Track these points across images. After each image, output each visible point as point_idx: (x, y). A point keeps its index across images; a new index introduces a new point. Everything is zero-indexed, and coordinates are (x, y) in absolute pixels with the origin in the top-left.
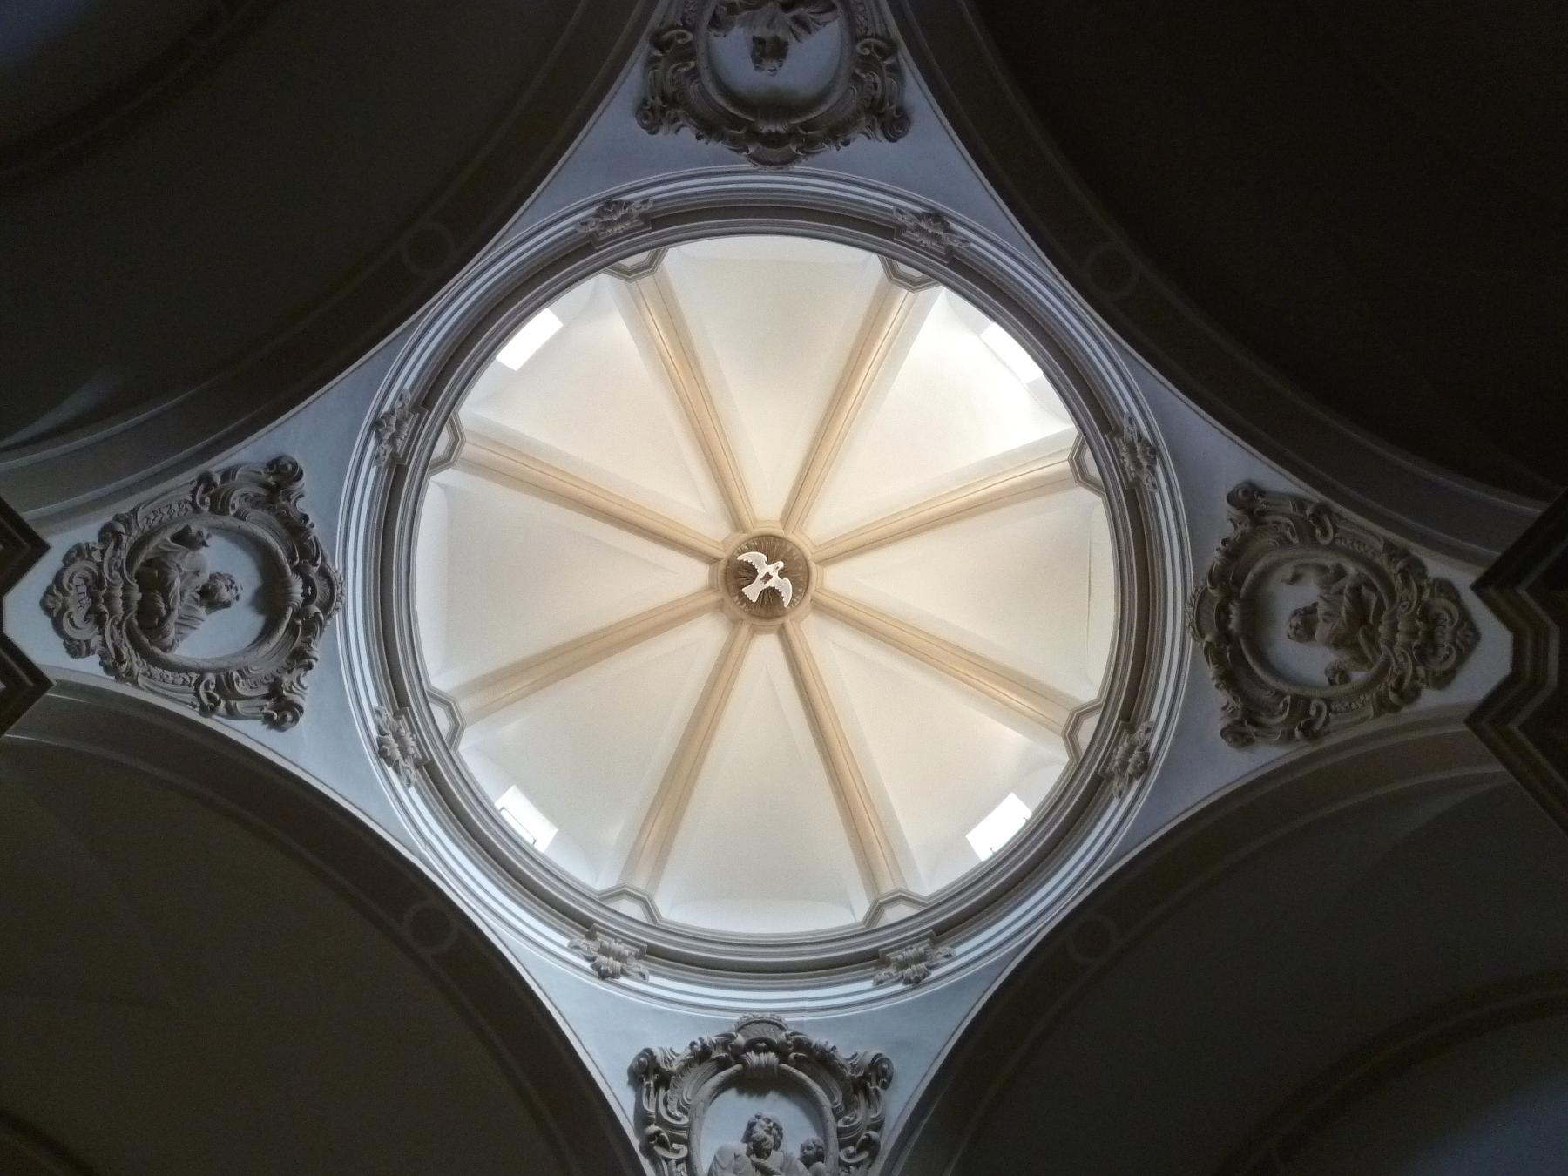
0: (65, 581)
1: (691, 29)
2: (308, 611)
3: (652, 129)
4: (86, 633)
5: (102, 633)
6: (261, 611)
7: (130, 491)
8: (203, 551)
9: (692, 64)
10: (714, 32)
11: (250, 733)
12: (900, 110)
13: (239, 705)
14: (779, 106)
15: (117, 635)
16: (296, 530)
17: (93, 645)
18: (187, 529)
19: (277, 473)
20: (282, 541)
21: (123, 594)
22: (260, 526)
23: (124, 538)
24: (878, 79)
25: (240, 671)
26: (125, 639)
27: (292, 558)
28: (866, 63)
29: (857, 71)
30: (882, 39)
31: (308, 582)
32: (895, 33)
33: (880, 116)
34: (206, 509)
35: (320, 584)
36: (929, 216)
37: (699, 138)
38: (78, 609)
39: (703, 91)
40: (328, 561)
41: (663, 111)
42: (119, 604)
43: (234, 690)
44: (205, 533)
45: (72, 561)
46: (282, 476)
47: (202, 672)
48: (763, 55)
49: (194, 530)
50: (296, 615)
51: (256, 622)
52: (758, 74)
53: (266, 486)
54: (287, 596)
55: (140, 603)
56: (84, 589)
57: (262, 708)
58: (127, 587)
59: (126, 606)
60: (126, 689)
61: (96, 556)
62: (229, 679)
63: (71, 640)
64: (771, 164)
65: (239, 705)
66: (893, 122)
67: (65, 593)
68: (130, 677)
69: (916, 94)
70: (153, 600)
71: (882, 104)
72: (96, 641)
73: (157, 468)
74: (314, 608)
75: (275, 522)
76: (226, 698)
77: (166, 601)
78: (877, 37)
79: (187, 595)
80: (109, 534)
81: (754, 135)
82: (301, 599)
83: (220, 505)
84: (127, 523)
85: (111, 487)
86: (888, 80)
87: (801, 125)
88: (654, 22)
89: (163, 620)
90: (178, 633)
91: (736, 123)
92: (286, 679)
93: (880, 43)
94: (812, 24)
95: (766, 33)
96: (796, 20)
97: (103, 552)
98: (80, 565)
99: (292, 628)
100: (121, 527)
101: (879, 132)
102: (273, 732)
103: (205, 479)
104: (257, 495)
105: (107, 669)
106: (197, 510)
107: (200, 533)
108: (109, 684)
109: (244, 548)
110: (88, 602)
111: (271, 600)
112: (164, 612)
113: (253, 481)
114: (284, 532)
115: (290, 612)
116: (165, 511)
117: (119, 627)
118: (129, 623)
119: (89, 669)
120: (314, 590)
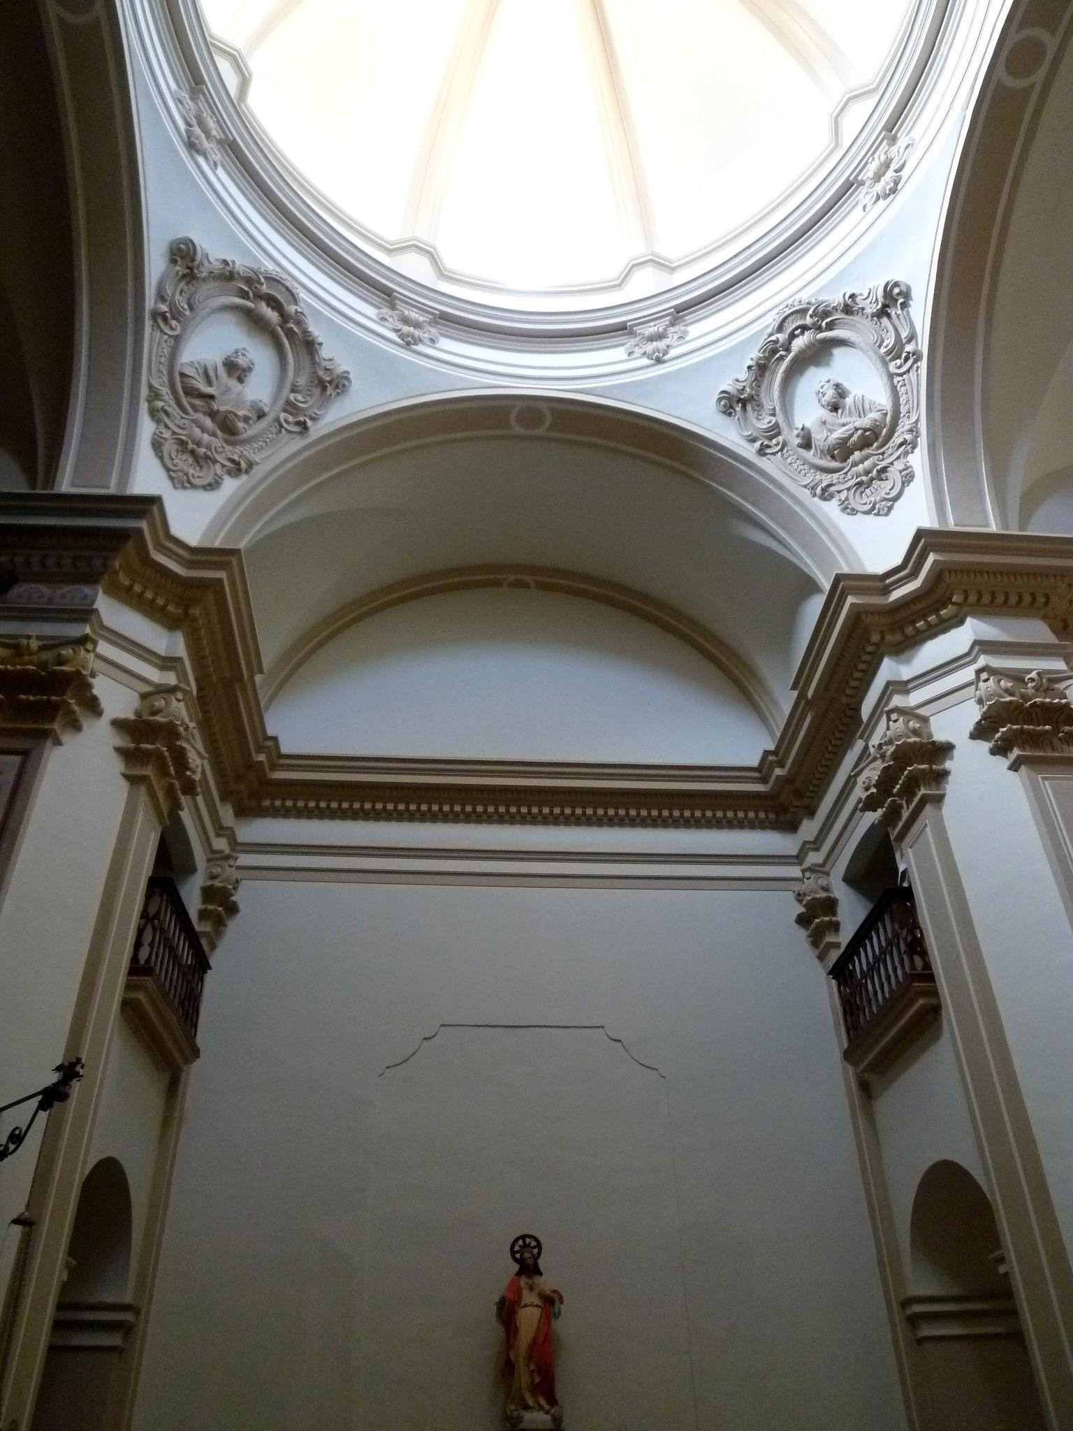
0: (868, 507)
1: (277, 420)
2: (814, 324)
3: (345, 377)
4: (894, 474)
5: (892, 463)
6: (831, 354)
7: (793, 497)
8: (808, 425)
9: (292, 397)
10: (266, 409)
11: (921, 312)
12: (174, 261)
13: (904, 335)
14: (254, 322)
15: (890, 452)
16: (761, 369)
17: (902, 467)
18: (800, 446)
19: (731, 407)
20: (774, 372)
21: (861, 463)
22: (772, 394)
23: (824, 485)
24: (177, 297)
25: (880, 346)
26: (890, 444)
27: (782, 358)
28: (177, 314)
29: (188, 313)
30: (159, 327)
31: (792, 336)
32: (148, 323)
33: (191, 269)
34: (780, 438)
35: (790, 327)
36: (198, 152)
37: (321, 344)
38: (882, 489)
39: (297, 372)
40: (769, 330)
41: (330, 382)
42: (867, 463)
43: (894, 347)
44: (795, 432)
45: (853, 510)
46: (734, 403)
47: (891, 376)
48: (244, 370)
49: (798, 441)
50: (819, 329)
51: (838, 353)
52: (256, 361)
53: (744, 407)
54: (810, 346)
55: (861, 449)
56: (868, 491)
57: (898, 316)
58: (855, 464)
59: (867, 458)
60: (923, 426)
61: (843, 495)
62: (888, 353)
63: (903, 483)
64: (287, 288)
65: (904, 335)
66: (184, 255)
67: (875, 504)
68: (914, 430)
69: (156, 265)
70: (855, 444)
71: (184, 276)
72: (899, 465)
73: (771, 487)
74: (808, 321)
75: (764, 386)
76: (903, 346)
77: (852, 435)
78: (162, 331)
79: (843, 420)
80: (826, 495)
81: (285, 317)
82: (807, 333)
83: (775, 431)
84: (813, 488)
85: (797, 509)
86: (169, 293)
87: (248, 299)
88: (298, 443)
89: (866, 430)
90: (871, 410)
91: (290, 334)
92: (869, 311)
93: (162, 325)
94: (201, 371)
95: (232, 383)
96: (210, 383)
97: (839, 492)
98: (853, 505)
99: (830, 326)
100: (819, 490)
101: (199, 257)
102: (913, 294)
103: (762, 452)
104: (754, 410)
105: (914, 448)
106: (785, 444)
107: (798, 436)
108: (923, 441)
109: (792, 397)
110: (876, 483)
111: (819, 353)
112: (860, 432)
113: (746, 419)
114: (767, 374)
115: (821, 336)
116: (795, 466)
117: (883, 454)
118: (878, 448)
119: (918, 460)
120: (796, 329)
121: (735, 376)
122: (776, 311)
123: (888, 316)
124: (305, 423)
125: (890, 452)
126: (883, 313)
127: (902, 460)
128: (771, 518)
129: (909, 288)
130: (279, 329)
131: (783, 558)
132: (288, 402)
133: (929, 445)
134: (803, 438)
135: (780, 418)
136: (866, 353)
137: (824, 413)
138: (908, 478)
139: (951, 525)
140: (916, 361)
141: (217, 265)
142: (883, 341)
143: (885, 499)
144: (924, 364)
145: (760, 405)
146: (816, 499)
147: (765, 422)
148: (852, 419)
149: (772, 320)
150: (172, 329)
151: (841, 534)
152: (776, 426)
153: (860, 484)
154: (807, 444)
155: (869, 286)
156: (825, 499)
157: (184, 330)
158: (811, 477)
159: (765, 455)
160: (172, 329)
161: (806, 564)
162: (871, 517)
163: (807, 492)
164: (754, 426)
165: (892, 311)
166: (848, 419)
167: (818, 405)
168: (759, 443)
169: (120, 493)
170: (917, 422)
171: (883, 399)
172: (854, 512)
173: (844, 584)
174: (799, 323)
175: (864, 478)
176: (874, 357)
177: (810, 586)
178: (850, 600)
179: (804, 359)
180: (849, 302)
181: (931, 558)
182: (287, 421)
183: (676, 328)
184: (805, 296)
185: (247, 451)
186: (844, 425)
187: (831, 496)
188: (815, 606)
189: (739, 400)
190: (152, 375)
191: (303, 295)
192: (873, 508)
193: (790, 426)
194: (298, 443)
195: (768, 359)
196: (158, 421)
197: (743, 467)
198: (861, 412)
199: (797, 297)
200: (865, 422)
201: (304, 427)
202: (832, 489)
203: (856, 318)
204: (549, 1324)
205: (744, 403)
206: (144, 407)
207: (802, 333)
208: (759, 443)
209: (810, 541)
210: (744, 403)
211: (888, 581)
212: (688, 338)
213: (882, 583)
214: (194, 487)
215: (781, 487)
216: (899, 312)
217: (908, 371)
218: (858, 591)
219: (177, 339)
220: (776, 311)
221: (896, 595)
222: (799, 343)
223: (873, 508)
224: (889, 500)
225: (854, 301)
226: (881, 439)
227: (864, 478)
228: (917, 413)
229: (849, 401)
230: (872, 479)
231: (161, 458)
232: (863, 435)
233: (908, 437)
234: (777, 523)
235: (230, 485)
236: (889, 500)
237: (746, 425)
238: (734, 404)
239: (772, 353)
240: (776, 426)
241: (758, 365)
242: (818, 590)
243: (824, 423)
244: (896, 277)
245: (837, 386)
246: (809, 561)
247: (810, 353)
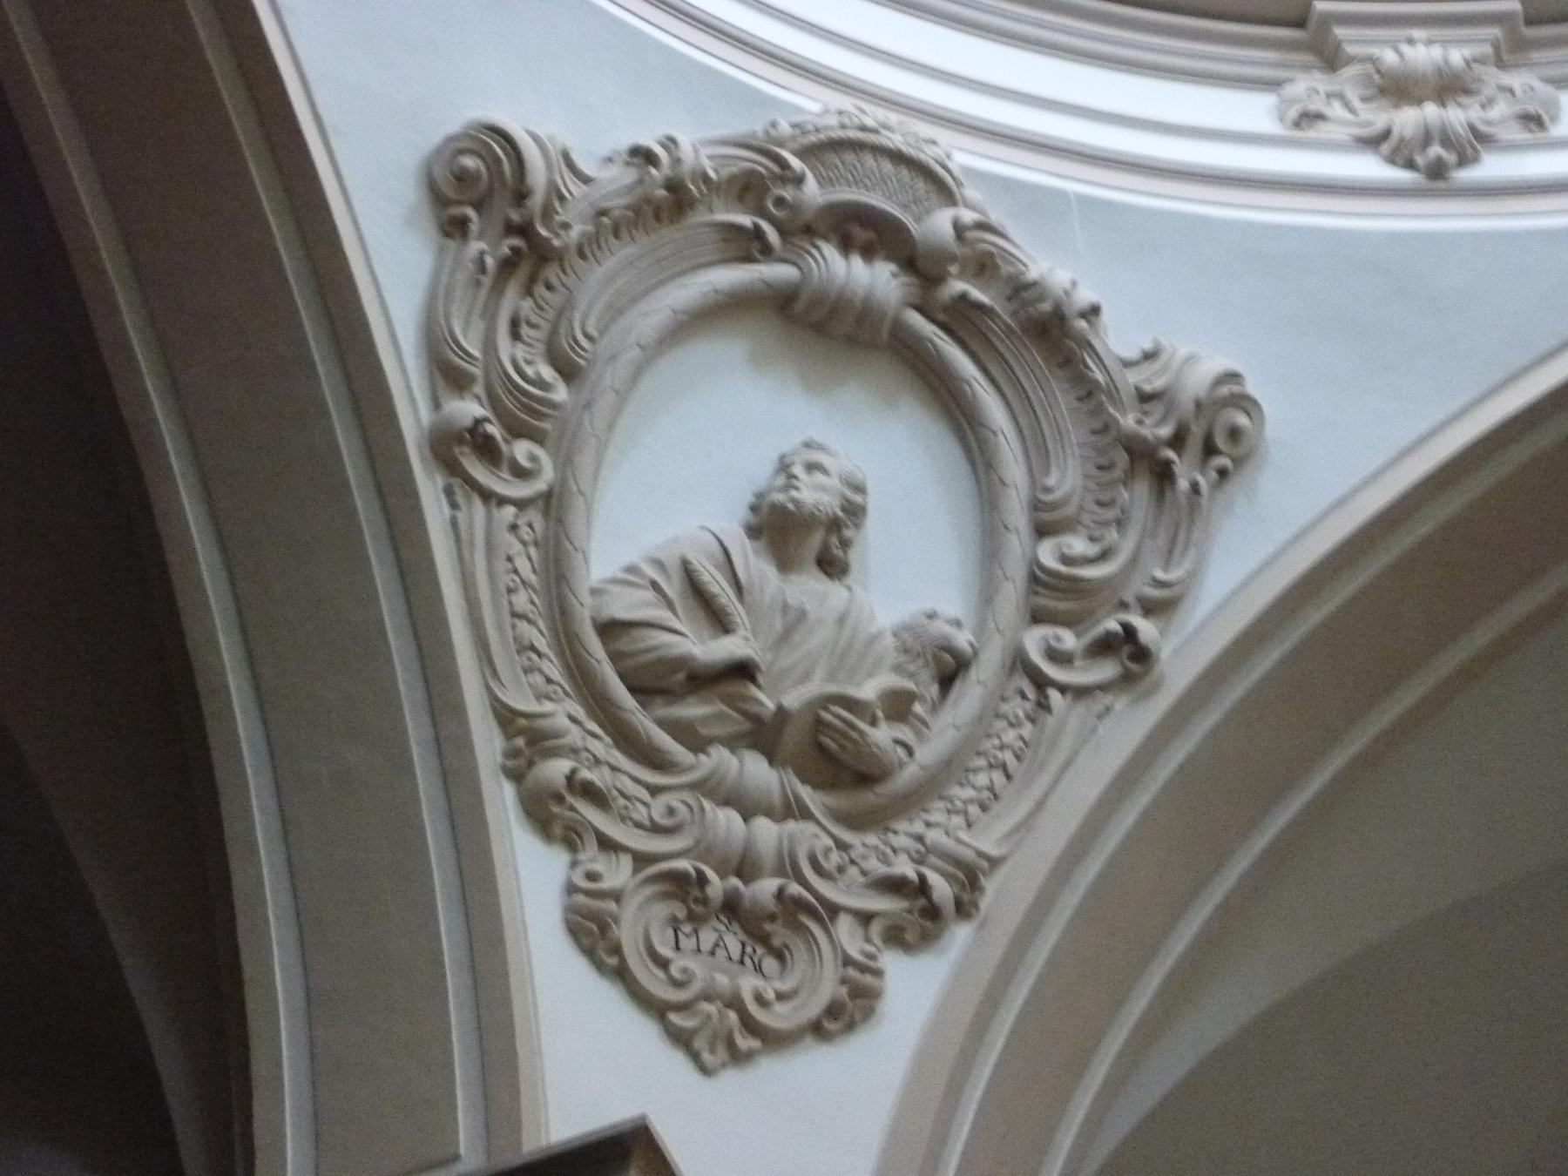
46: (484, 193)
78: (487, 496)
97: (607, 845)
124: (1129, 632)
130: (916, 319)
132: (1039, 579)
133: (480, 607)
141: (615, 180)
150: (520, 473)
155: (1150, 325)
157: (565, 463)
160: (520, 473)
182: (1057, 656)
185: (940, 826)
190: (498, 670)
191: (962, 156)
194: (1129, 725)
196: (571, 838)
201: (1129, 651)
206: (502, 802)
214: (775, 1041)
219: (552, 503)
224: (750, 1026)
230: (732, 908)
231: (621, 975)
235: (915, 986)
241: (674, 186)
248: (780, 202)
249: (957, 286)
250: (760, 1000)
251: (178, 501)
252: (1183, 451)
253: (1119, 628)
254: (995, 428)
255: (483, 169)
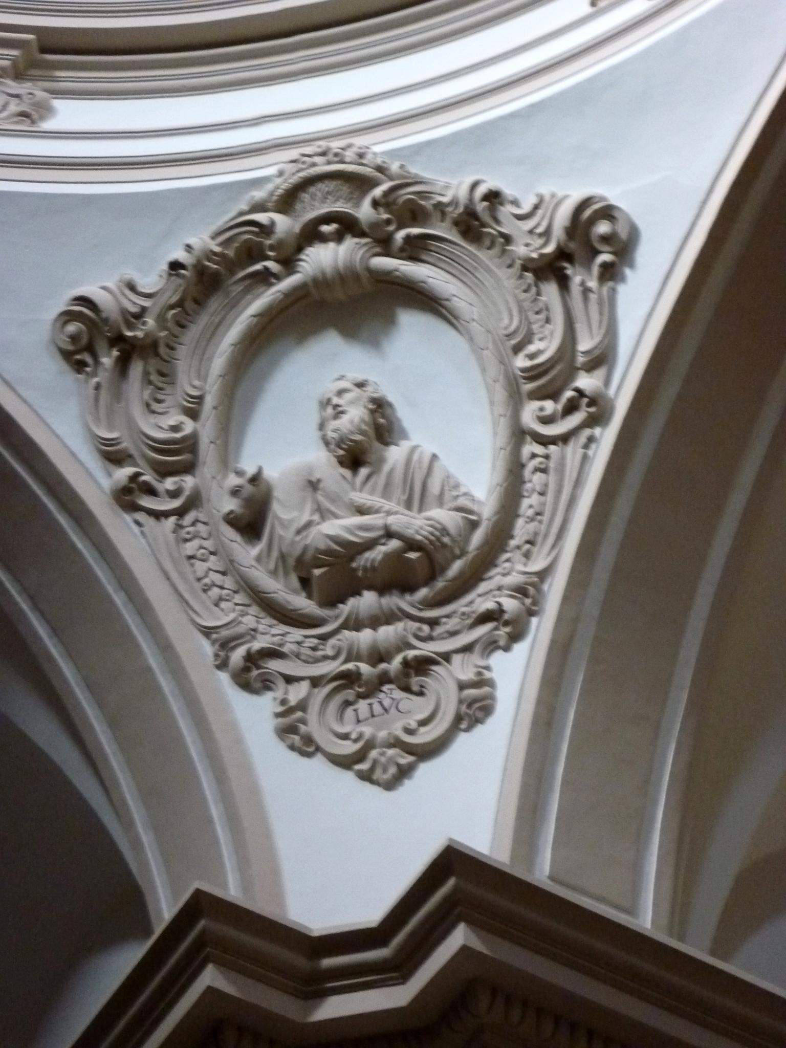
0: (348, 748)
2: (376, 226)
4: (444, 686)
5: (447, 657)
6: (390, 321)
7: (166, 648)
8: (271, 473)
11: (643, 304)
13: (585, 344)
15: (451, 624)
16: (204, 283)
17: (468, 675)
18: (232, 520)
19: (90, 348)
20: (234, 305)
21: (373, 626)
22: (205, 363)
23: (256, 645)
25: (517, 349)
26: (459, 606)
27: (266, 278)
31: (311, 235)
34: (188, 482)
35: (314, 207)
38: (399, 714)
40: (259, 194)
42: (387, 633)
44: (233, 481)
45: (308, 740)
46: (98, 340)
47: (520, 434)
49: (231, 505)
50: (385, 245)
51: (411, 324)
53: (123, 364)
54: (345, 277)
55: (383, 590)
56: (362, 705)
57: (586, 291)
59: (389, 618)
62: (533, 374)
63: (458, 719)
65: (585, 344)
68: (529, 592)
72: (463, 669)
74: (365, 212)
75: (194, 331)
76: (572, 372)
77: (370, 545)
79: (362, 498)
80: (253, 674)
82: (350, 242)
83: (178, 456)
84: (227, 645)
85: (165, 683)
89: (411, 545)
90: (440, 501)
92: (520, 250)
97: (290, 680)
98: (314, 727)
99: (415, 249)
100: (237, 656)
103: (127, 497)
105: (516, 637)
106: (194, 501)
108: (542, 629)
110: (391, 694)
111: (364, 306)
113: (117, 395)
114: (215, 303)
117: (433, 623)
119: (515, 673)
120: (327, 219)
121: (130, 272)
122: (294, 153)
123: (563, 282)
125: (451, 624)
126: (551, 269)
127: (476, 659)
128: (91, 687)
129: (634, 234)
131: (101, 828)
133: (553, 643)
134: (249, 502)
135: (206, 430)
136: (477, 350)
137: (320, 460)
138: (475, 709)
139: (542, 872)
140: (593, 421)
142: (528, 339)
143: (397, 743)
144: (607, 437)
145: (167, 375)
146: (224, 677)
147: (165, 424)
148: (387, 505)
149: (272, 172)
151: (254, 791)
152: (190, 445)
153: (348, 679)
154: (252, 521)
155: (544, 188)
156: (246, 686)
158: (225, 614)
159: (133, 508)
161: (136, 843)
162: (347, 778)
163: (208, 648)
164: (131, 423)
165: (576, 276)
166: (387, 505)
167: (315, 435)
168: (126, 472)
169: (519, 872)
170: (543, 575)
171: (481, 486)
172: (307, 747)
173: (217, 927)
174: (340, 207)
175: (365, 668)
176: (494, 369)
177: (130, 903)
178: (210, 977)
179: (321, 304)
180: (481, 207)
181: (459, 937)
183: (23, 88)
184: (380, 146)
186: (361, 511)
187: (266, 685)
188: (125, 960)
189: (118, 340)
192: (360, 757)
193: (226, 461)
195: (232, 265)
197: (63, 520)
198: (416, 496)
199: (359, 141)
200: (416, 524)
202: (275, 665)
203: (483, 255)
204: (300, 249)
205: (129, 351)
207: (338, 237)
208: (126, 472)
209: (171, 789)
210: (129, 351)
211: (328, 962)
212: (48, 125)
213: (313, 961)
215: (143, 609)
216: (593, 284)
217: (564, 439)
218: (235, 960)
220: (294, 153)
221: (337, 1007)
222: (322, 258)
223: (360, 757)
224: (408, 749)
225: (492, 210)
226: (440, 584)
227: (365, 668)
228: (553, 552)
229: (395, 455)
230: (385, 679)
232: (396, 557)
233: (510, 605)
234: (101, 704)
236: (408, 749)
237: (111, 413)
238: (101, 346)
239: (244, 255)
240: (190, 445)
241: (200, 270)
242: (145, 929)
243: (314, 485)
244: (613, 195)
245: (379, 406)
246: (146, 838)
247: (340, 295)
248: (272, 248)
249: (400, 235)
250: (410, 732)
251: (16, 604)
252: (591, 244)
253: (485, 203)
254: (446, 297)
255: (80, 325)
